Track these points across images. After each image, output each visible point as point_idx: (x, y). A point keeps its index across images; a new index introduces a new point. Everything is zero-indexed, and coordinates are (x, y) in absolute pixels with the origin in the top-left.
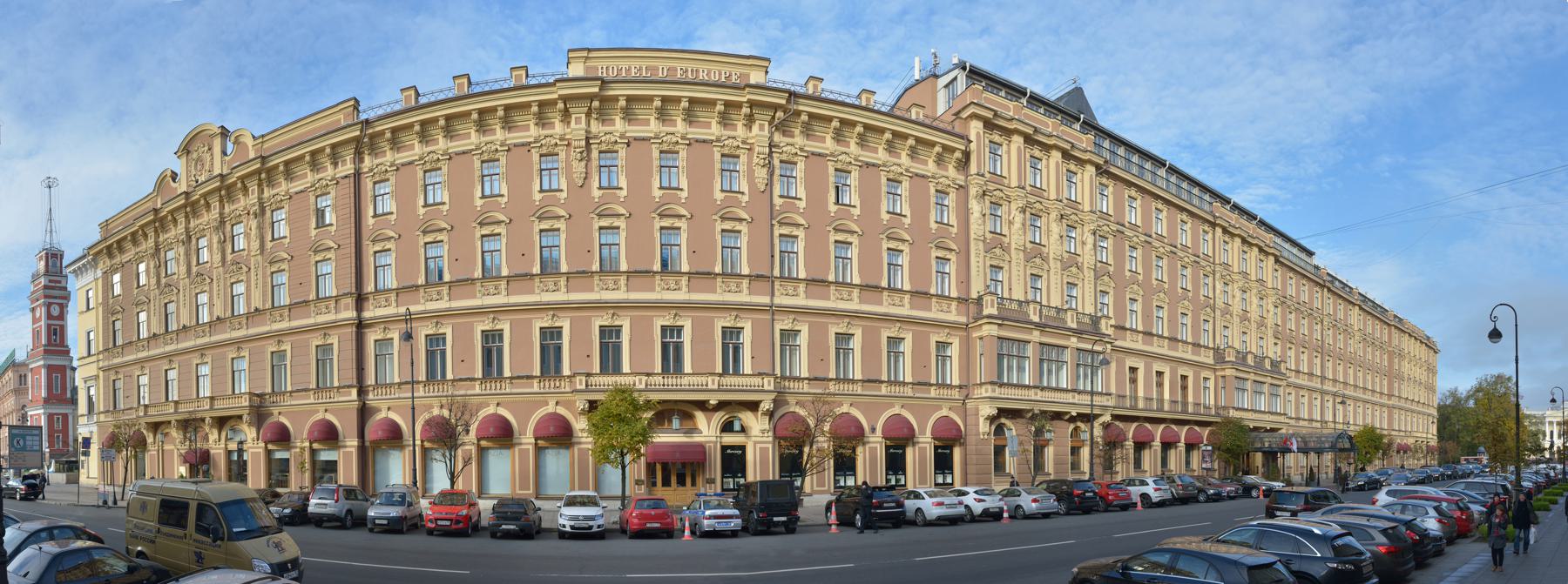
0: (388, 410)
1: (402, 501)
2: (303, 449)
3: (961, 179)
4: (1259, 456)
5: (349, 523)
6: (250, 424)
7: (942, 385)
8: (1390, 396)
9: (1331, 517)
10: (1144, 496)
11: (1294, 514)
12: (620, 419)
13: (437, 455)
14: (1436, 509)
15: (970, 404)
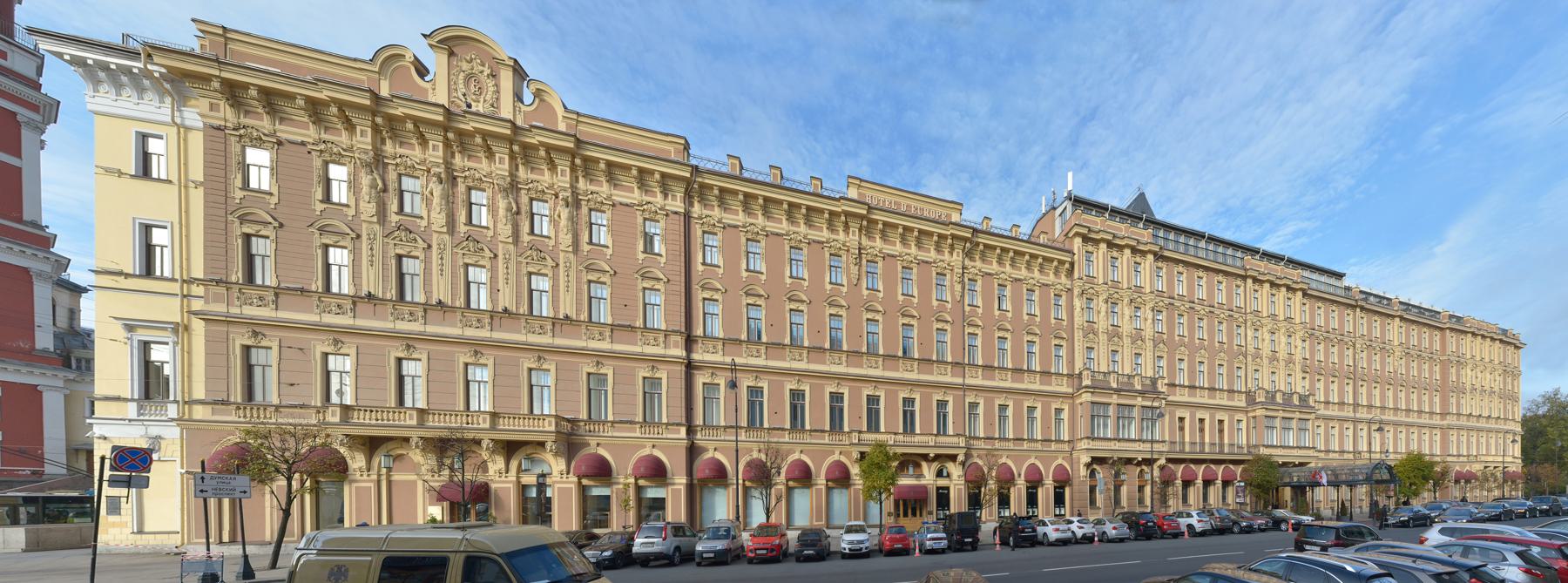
0: (715, 450)
1: (728, 534)
2: (627, 485)
3: (1068, 284)
4: (1288, 491)
5: (677, 559)
6: (556, 454)
7: (1059, 441)
8: (1443, 415)
9: (1366, 555)
10: (1190, 526)
11: (1324, 549)
12: (879, 467)
13: (756, 493)
14: (1519, 554)
15: (1075, 454)
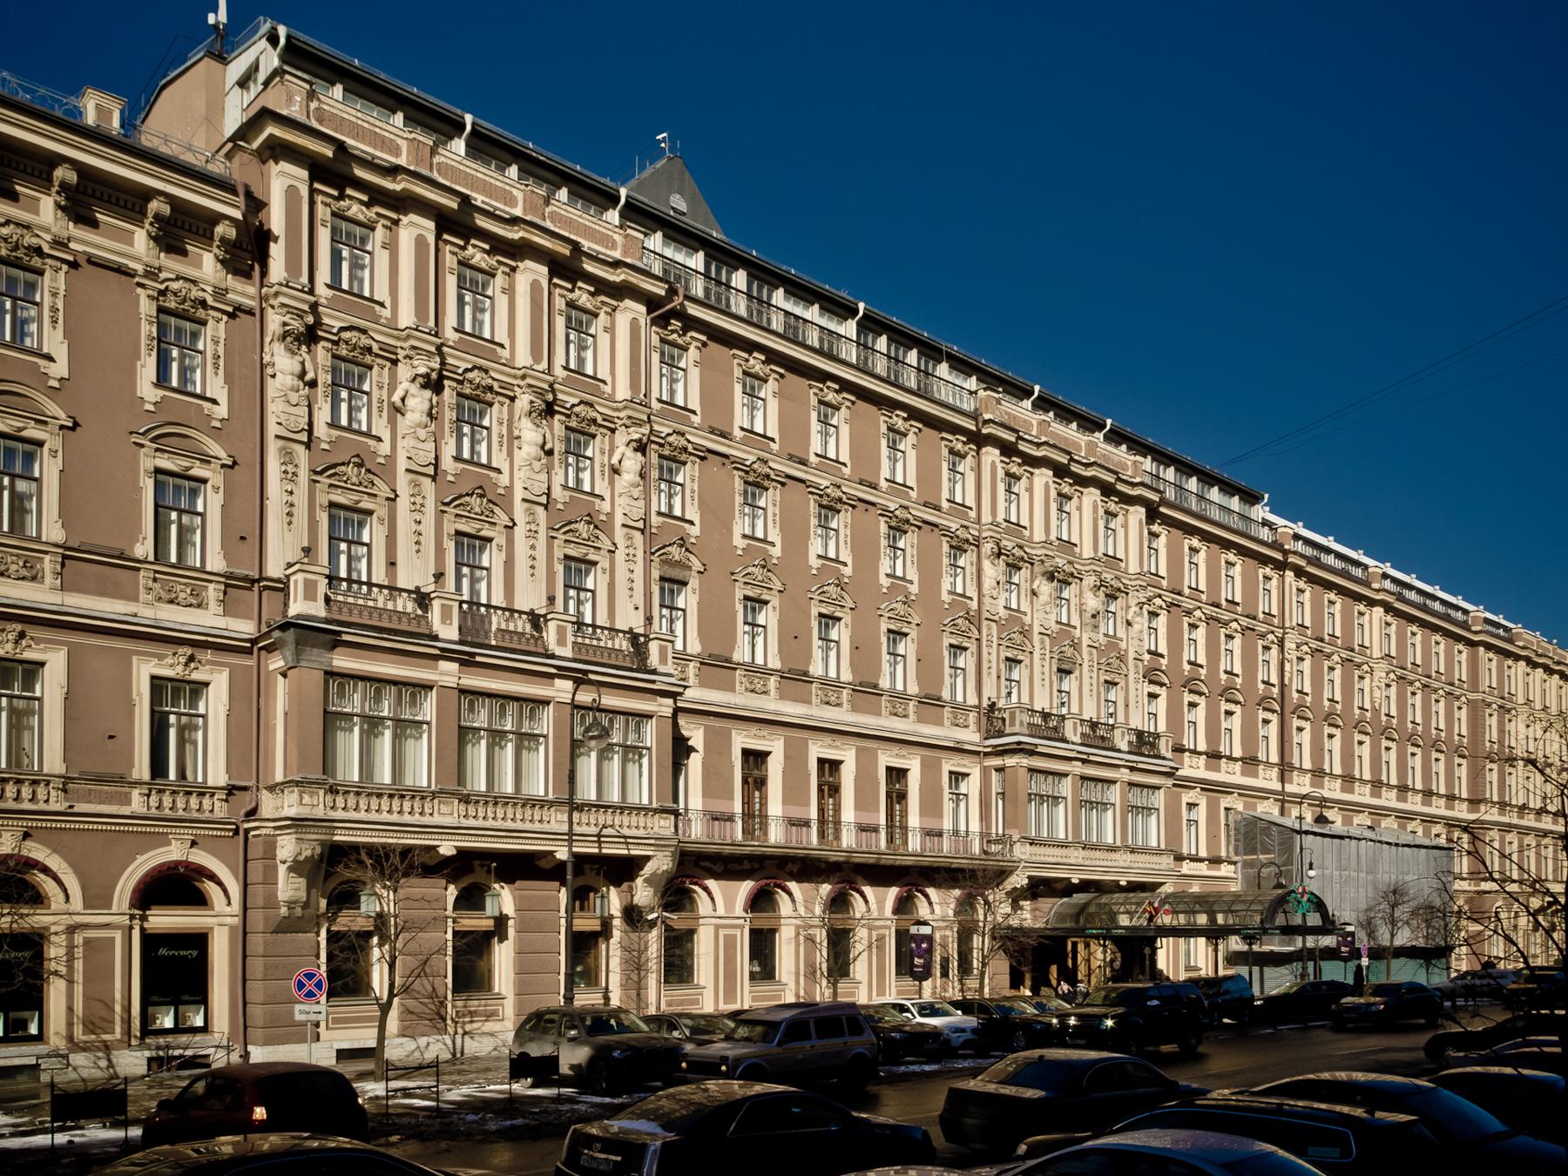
8: (1474, 802)
